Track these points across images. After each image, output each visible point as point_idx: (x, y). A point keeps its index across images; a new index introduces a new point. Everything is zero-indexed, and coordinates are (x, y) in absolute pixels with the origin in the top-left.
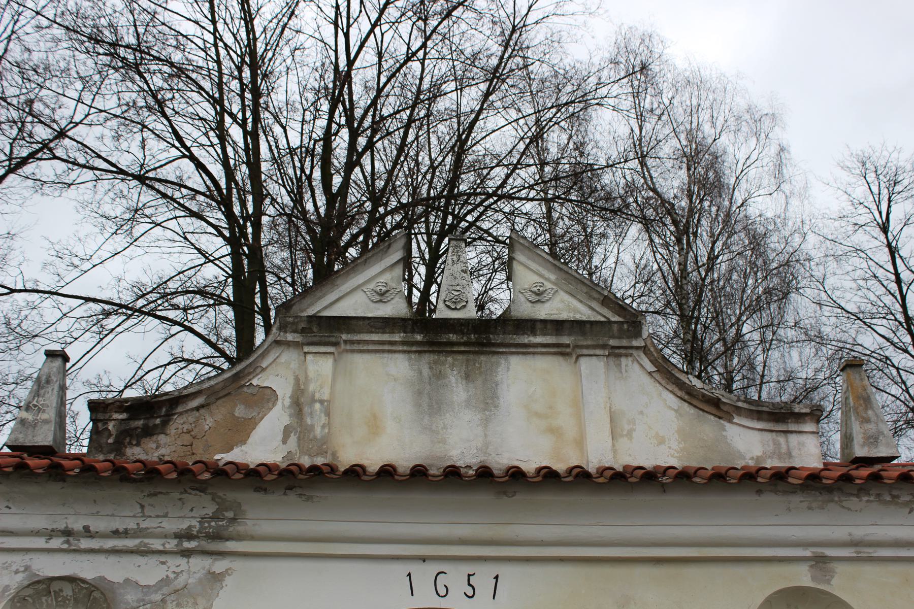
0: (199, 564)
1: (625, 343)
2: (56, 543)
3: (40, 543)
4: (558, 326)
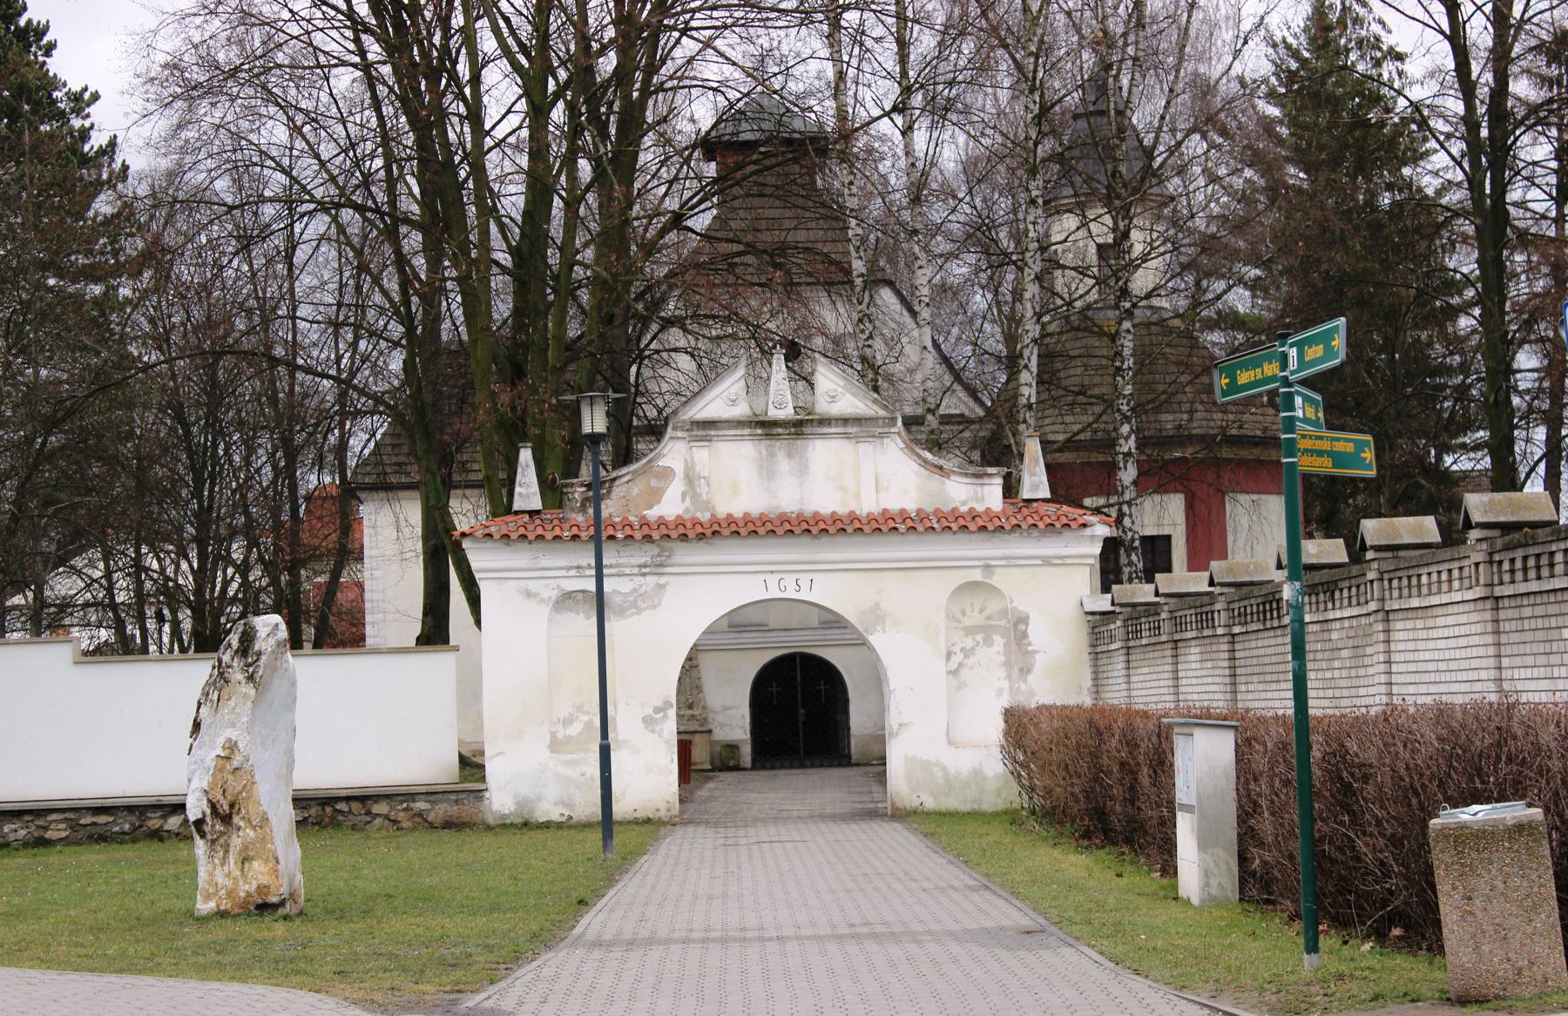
0: (651, 580)
1: (886, 430)
2: (572, 573)
3: (564, 573)
4: (845, 421)
